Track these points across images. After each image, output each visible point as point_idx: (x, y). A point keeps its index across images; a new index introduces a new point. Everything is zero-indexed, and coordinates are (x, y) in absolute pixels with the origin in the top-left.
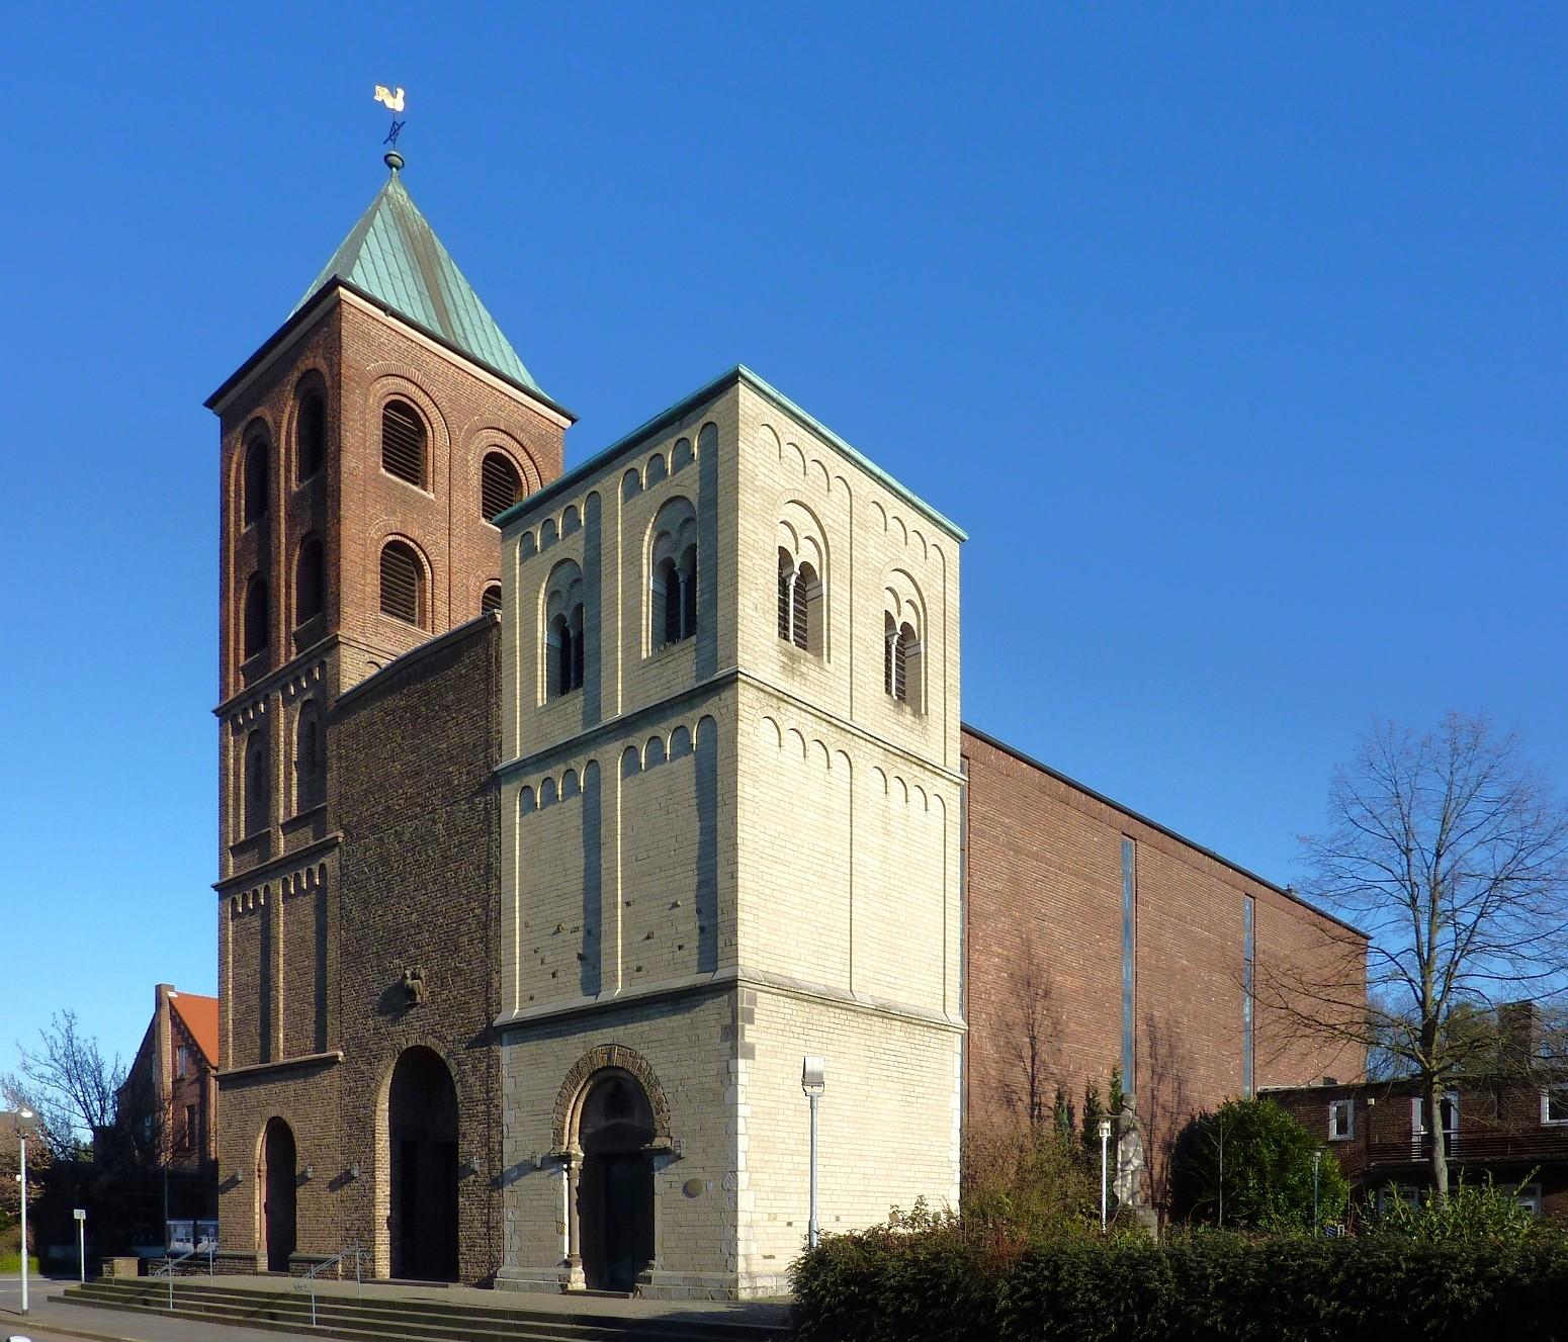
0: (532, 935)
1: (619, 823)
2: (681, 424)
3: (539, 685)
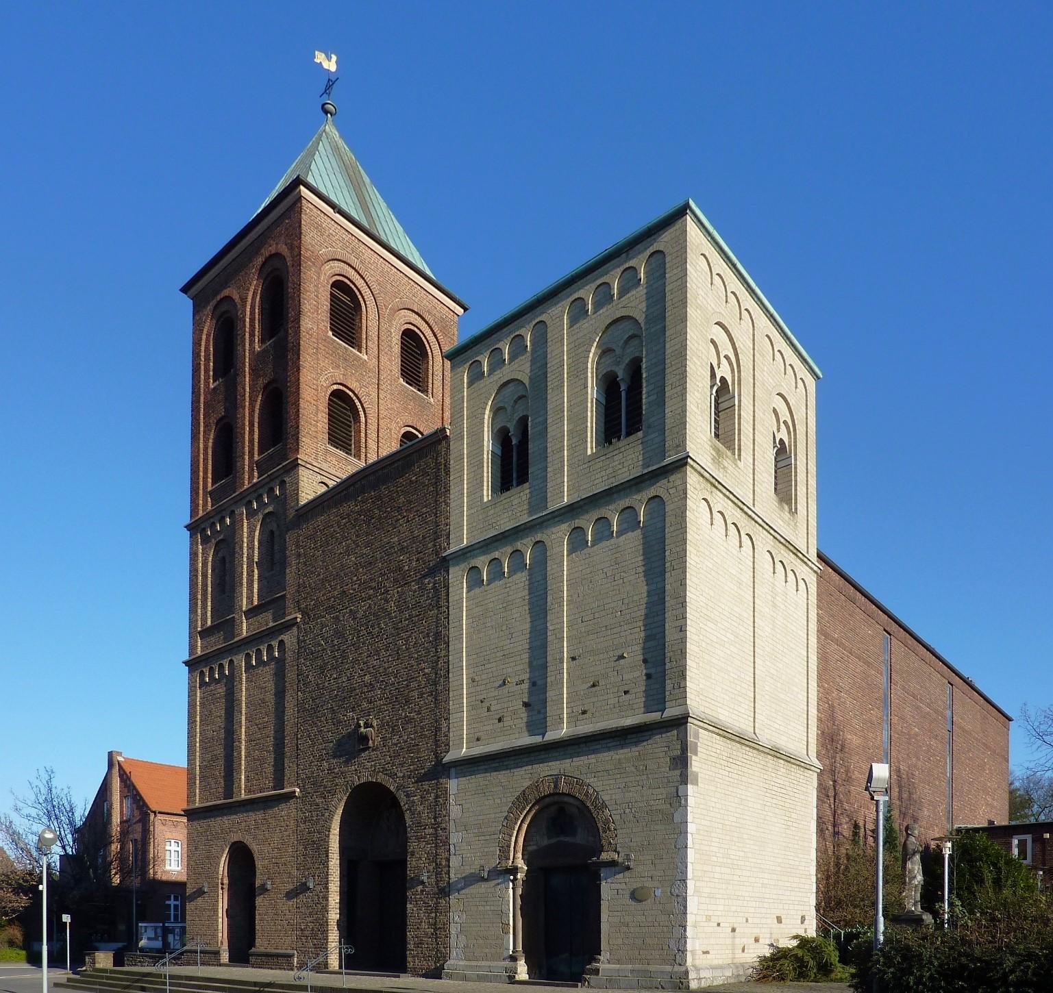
0: (478, 689)
1: (565, 592)
2: (627, 255)
3: (485, 484)
